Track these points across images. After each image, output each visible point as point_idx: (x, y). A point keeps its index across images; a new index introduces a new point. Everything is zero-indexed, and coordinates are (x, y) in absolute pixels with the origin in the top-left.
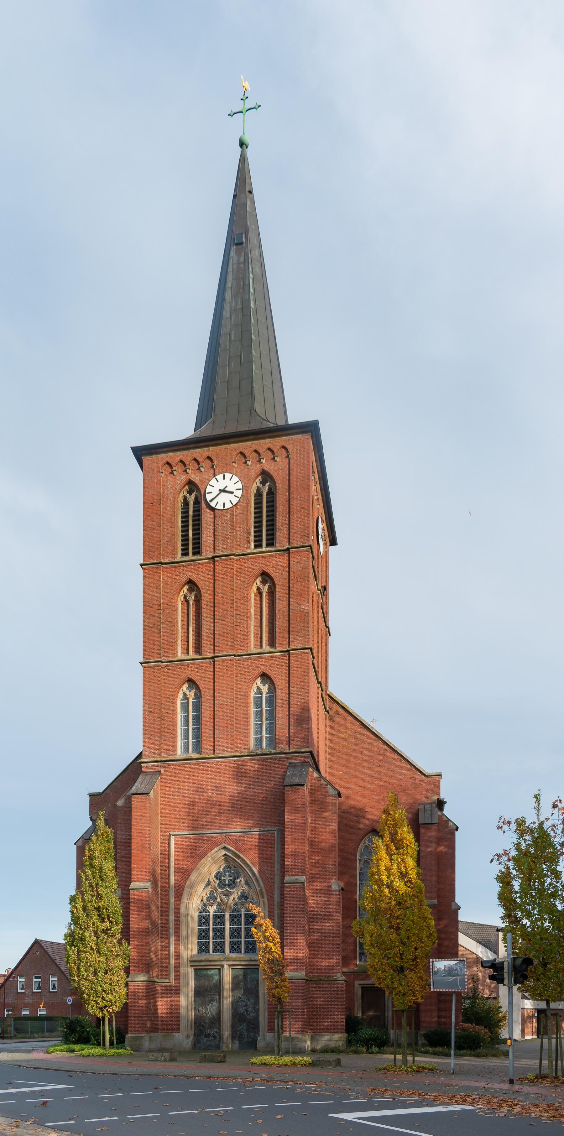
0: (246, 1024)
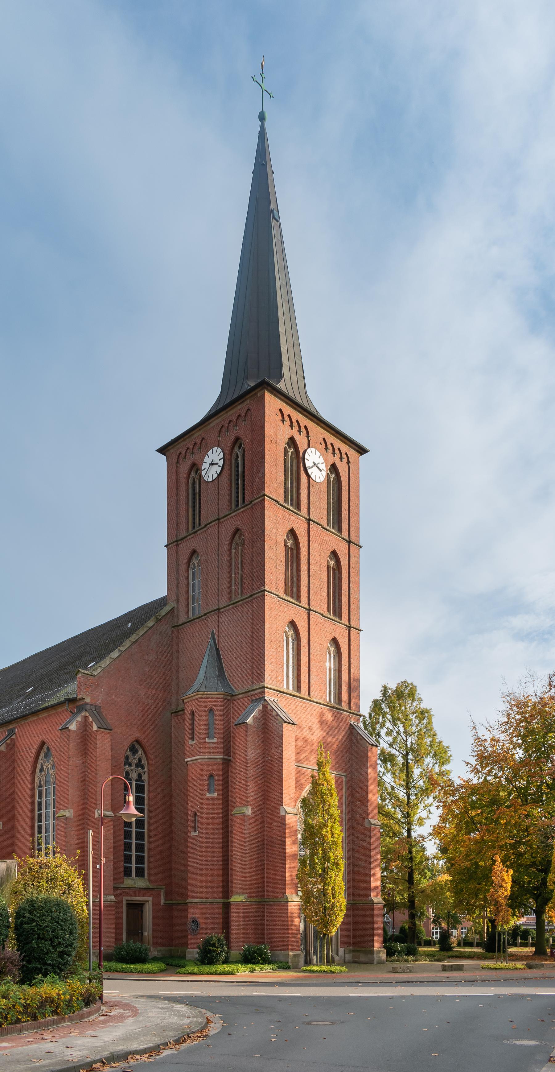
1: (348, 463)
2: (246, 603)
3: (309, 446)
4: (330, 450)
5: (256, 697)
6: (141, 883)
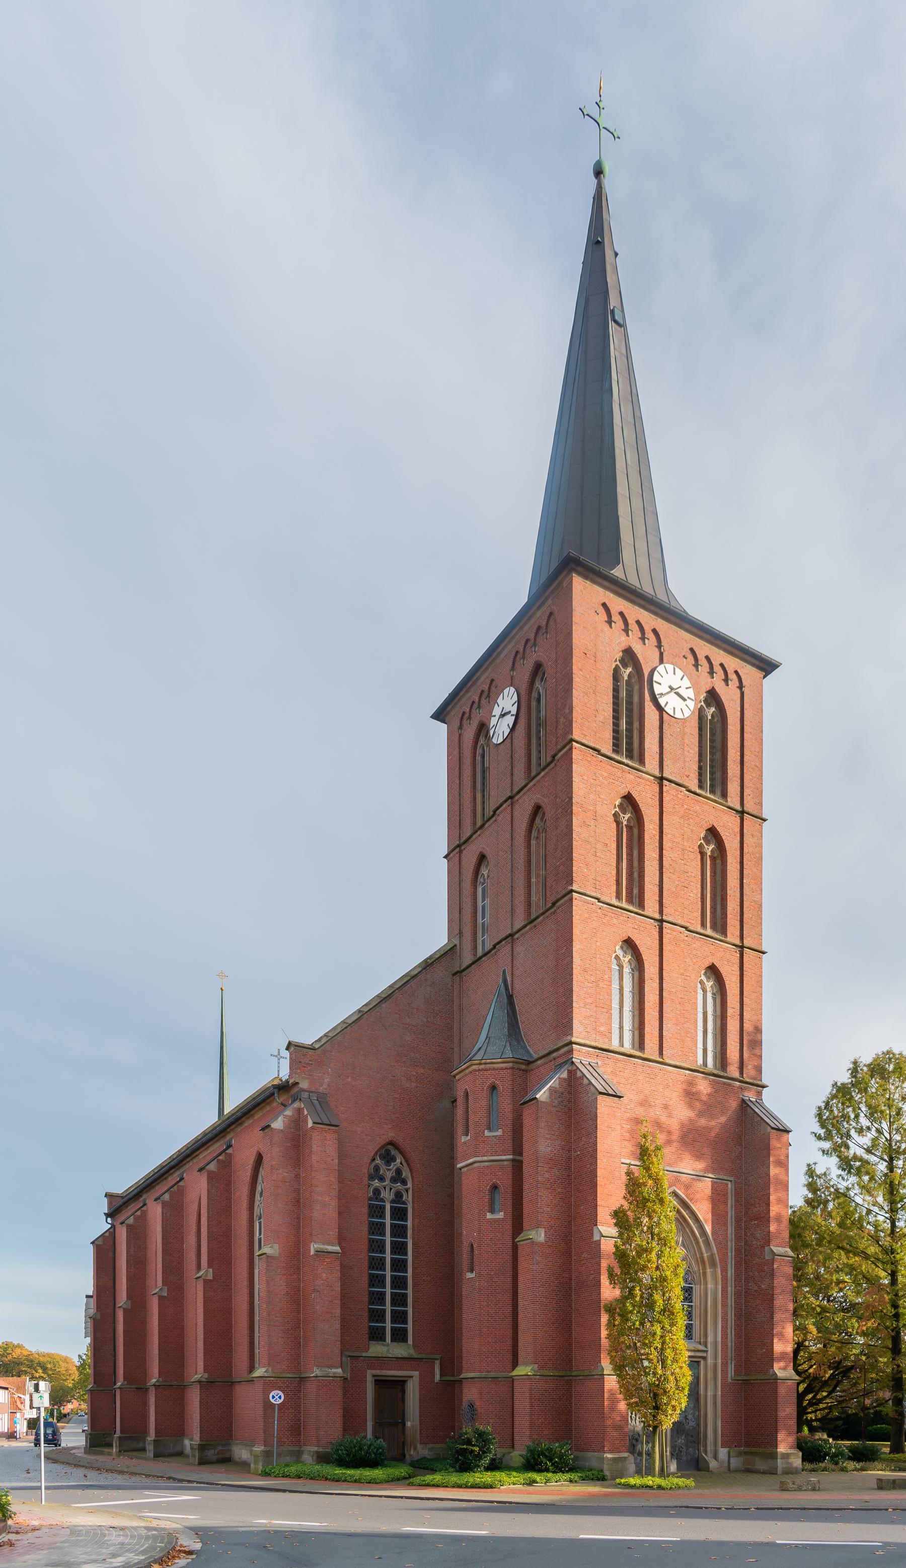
0: (685, 1437)
1: (741, 687)
3: (661, 661)
5: (561, 1061)
6: (399, 1350)
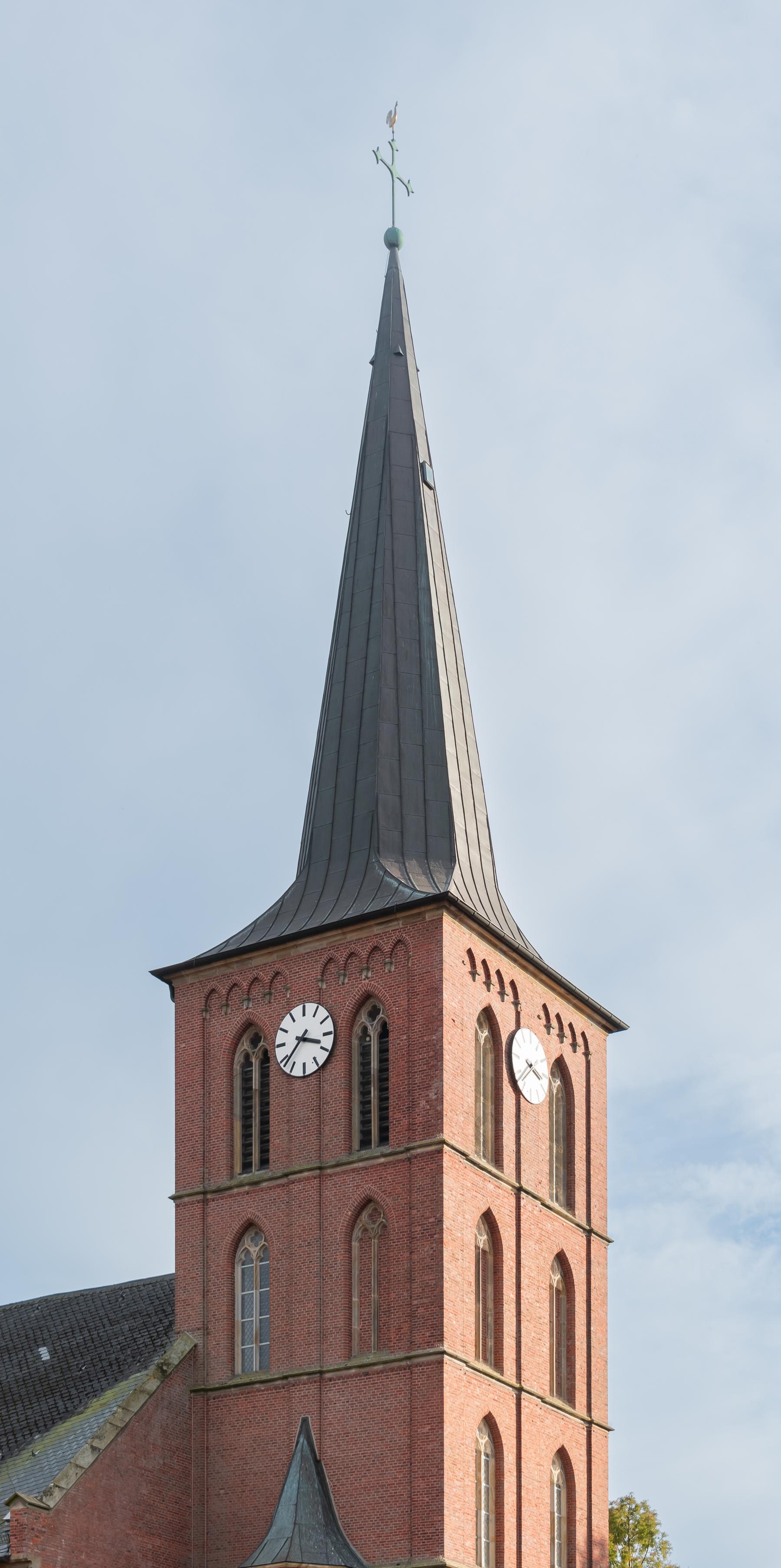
1: (587, 1054)
2: (392, 1370)
4: (555, 1031)
